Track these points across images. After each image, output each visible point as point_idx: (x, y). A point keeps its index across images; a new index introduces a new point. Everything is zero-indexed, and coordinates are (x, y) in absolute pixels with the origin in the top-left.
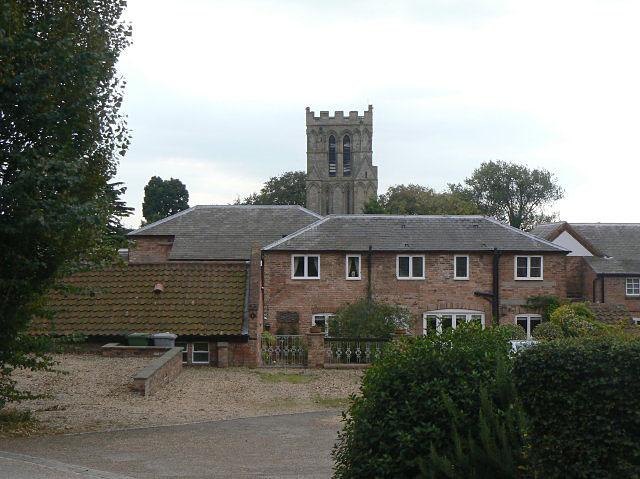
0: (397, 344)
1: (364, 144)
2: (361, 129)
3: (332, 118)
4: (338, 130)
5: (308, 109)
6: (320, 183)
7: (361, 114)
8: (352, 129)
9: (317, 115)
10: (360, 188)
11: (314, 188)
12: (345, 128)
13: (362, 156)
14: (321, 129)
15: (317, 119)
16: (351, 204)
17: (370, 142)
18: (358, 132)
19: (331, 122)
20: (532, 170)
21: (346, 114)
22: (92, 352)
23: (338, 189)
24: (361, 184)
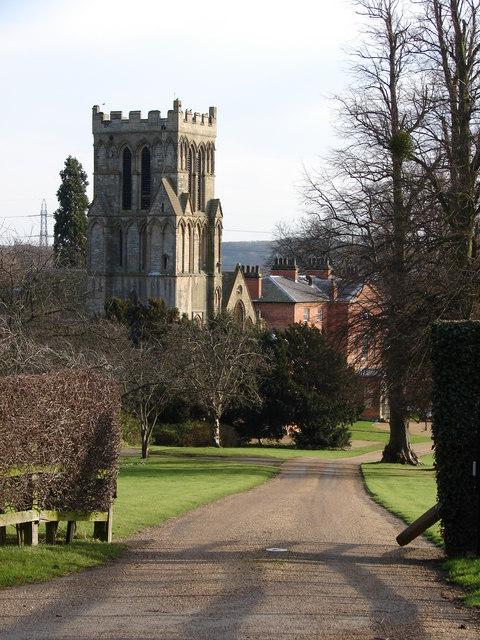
2: (164, 137)
4: (134, 140)
5: (95, 108)
8: (151, 139)
14: (111, 138)
15: (107, 123)
18: (158, 141)
19: (125, 128)
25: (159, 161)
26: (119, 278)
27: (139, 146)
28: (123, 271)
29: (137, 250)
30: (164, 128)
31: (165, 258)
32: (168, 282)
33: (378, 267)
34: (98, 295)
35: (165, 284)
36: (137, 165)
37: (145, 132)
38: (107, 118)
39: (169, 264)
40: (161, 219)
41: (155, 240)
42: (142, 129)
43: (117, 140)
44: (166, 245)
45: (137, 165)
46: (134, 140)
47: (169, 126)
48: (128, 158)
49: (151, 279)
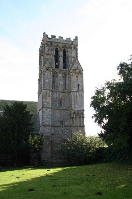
0: (80, 160)
1: (74, 54)
2: (73, 46)
3: (56, 39)
4: (61, 45)
5: (44, 33)
6: (51, 69)
7: (72, 39)
8: (68, 46)
9: (50, 36)
10: (74, 74)
11: (47, 72)
12: (64, 45)
13: (73, 59)
14: (51, 43)
15: (49, 38)
16: (67, 83)
17: (77, 53)
18: (71, 48)
19: (57, 41)
20: (97, 136)
21: (65, 39)
22: (51, 176)
23: (60, 75)
24: (74, 72)
25: (70, 54)
26: (55, 93)
27: (62, 48)
28: (55, 91)
29: (62, 83)
30: (72, 43)
31: (78, 85)
32: (81, 94)
33: (47, 139)
34: (48, 98)
35: (80, 95)
36: (61, 54)
37: (65, 44)
38: (50, 36)
39: (80, 88)
40: (77, 71)
41: (74, 78)
42: (64, 42)
43: (54, 44)
44: (79, 81)
45: (61, 54)
46: (61, 45)
47: (74, 43)
48: (57, 51)
49: (73, 93)
